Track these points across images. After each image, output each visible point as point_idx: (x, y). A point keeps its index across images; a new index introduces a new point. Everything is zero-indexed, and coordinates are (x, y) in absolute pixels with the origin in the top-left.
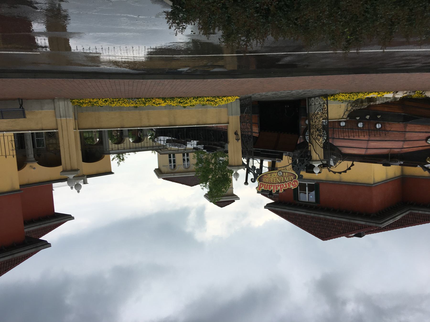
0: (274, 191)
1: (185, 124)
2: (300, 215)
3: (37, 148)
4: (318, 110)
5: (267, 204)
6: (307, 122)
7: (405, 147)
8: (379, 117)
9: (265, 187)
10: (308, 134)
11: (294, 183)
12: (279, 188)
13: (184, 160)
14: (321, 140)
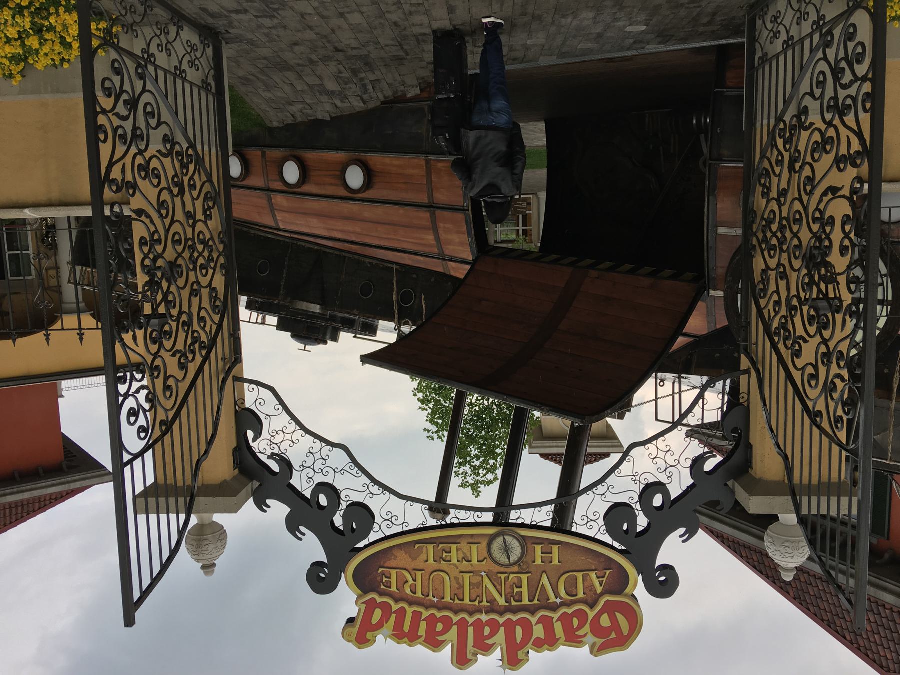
3: (10, 278)
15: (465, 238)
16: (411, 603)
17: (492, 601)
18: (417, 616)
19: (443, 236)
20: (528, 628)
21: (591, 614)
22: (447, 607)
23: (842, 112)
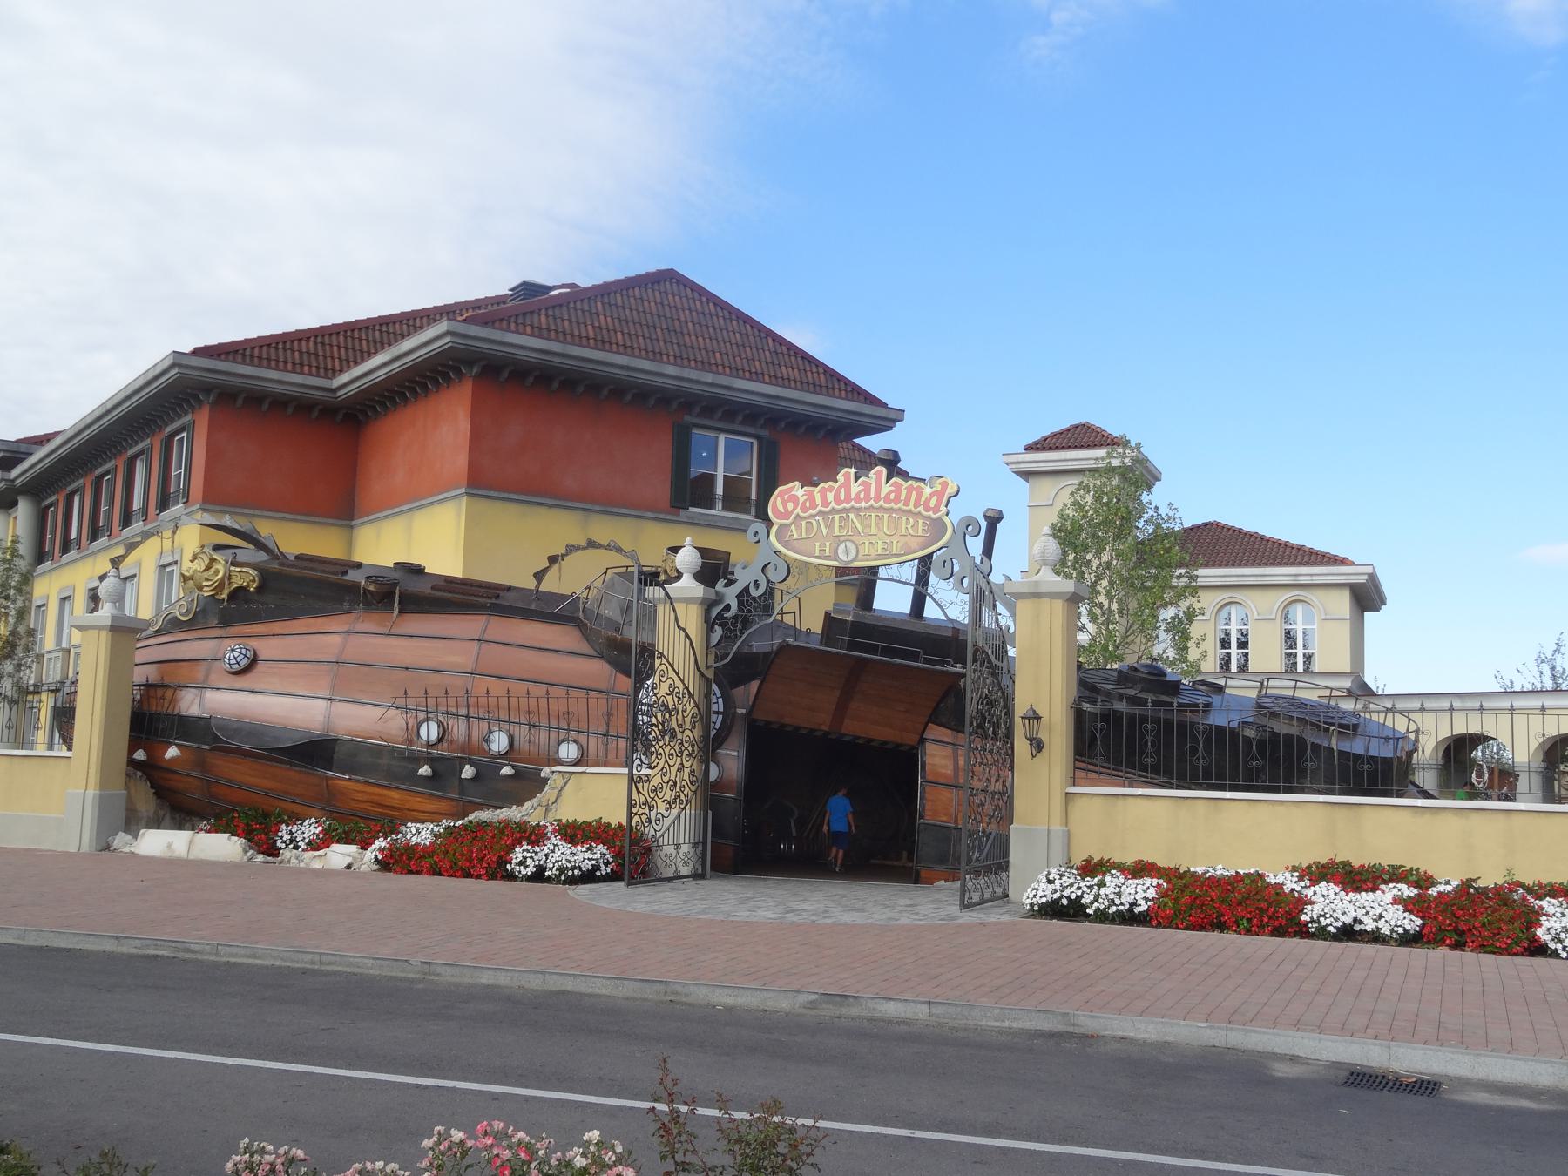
0: (879, 474)
1: (1281, 809)
2: (757, 376)
4: (667, 822)
5: (890, 428)
6: (714, 773)
7: (337, 639)
8: (425, 770)
9: (919, 494)
10: (714, 717)
11: (790, 506)
12: (855, 488)
13: (1243, 645)
14: (660, 687)
15: (928, 760)
16: (910, 512)
17: (858, 516)
18: (907, 503)
19: (950, 764)
20: (837, 500)
21: (798, 510)
22: (886, 510)
23: (646, 803)
